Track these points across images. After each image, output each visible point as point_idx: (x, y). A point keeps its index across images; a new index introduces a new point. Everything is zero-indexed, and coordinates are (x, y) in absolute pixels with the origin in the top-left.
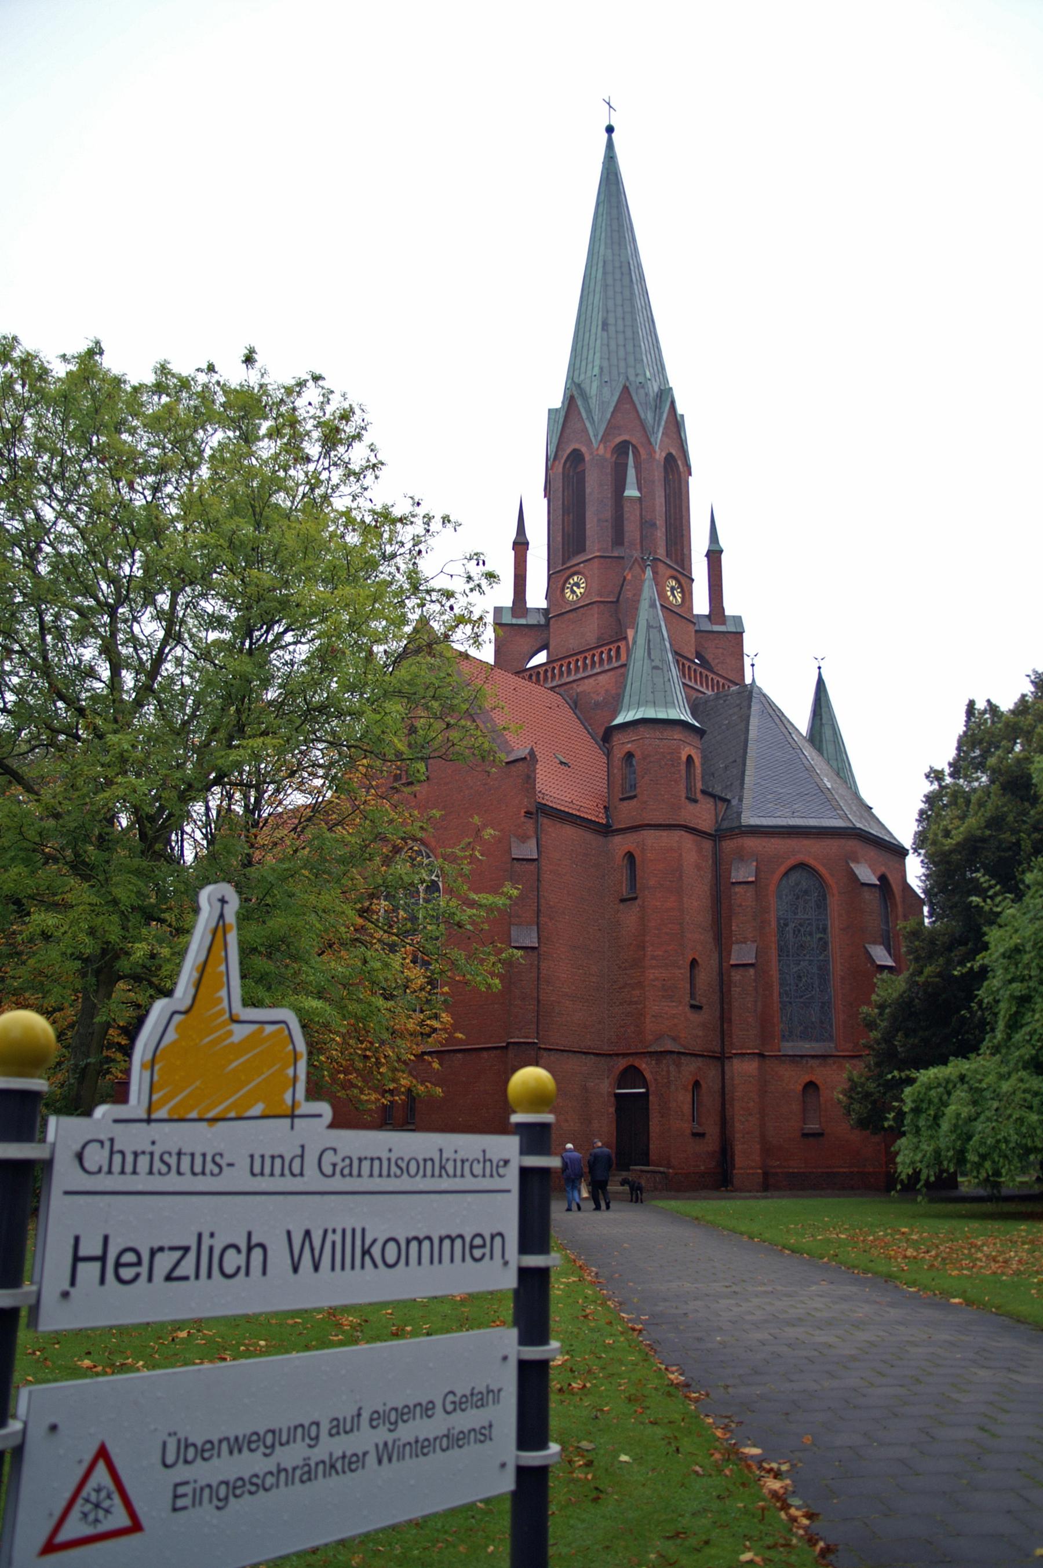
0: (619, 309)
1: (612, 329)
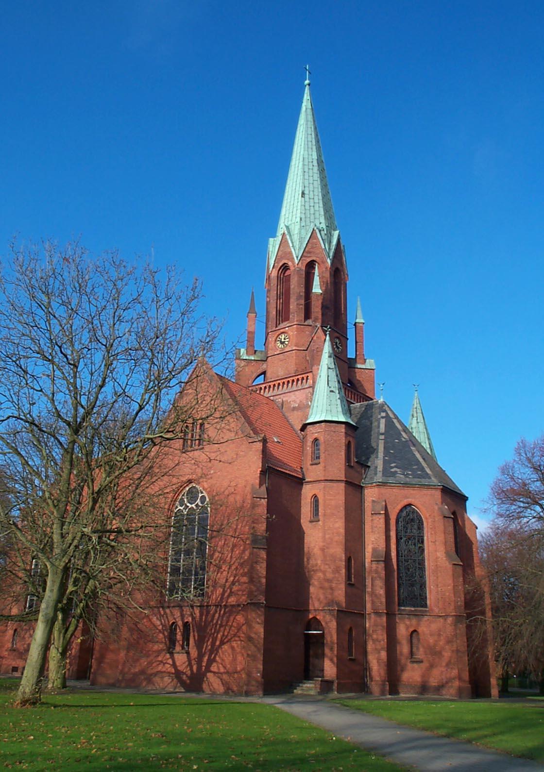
0: (311, 186)
1: (307, 196)
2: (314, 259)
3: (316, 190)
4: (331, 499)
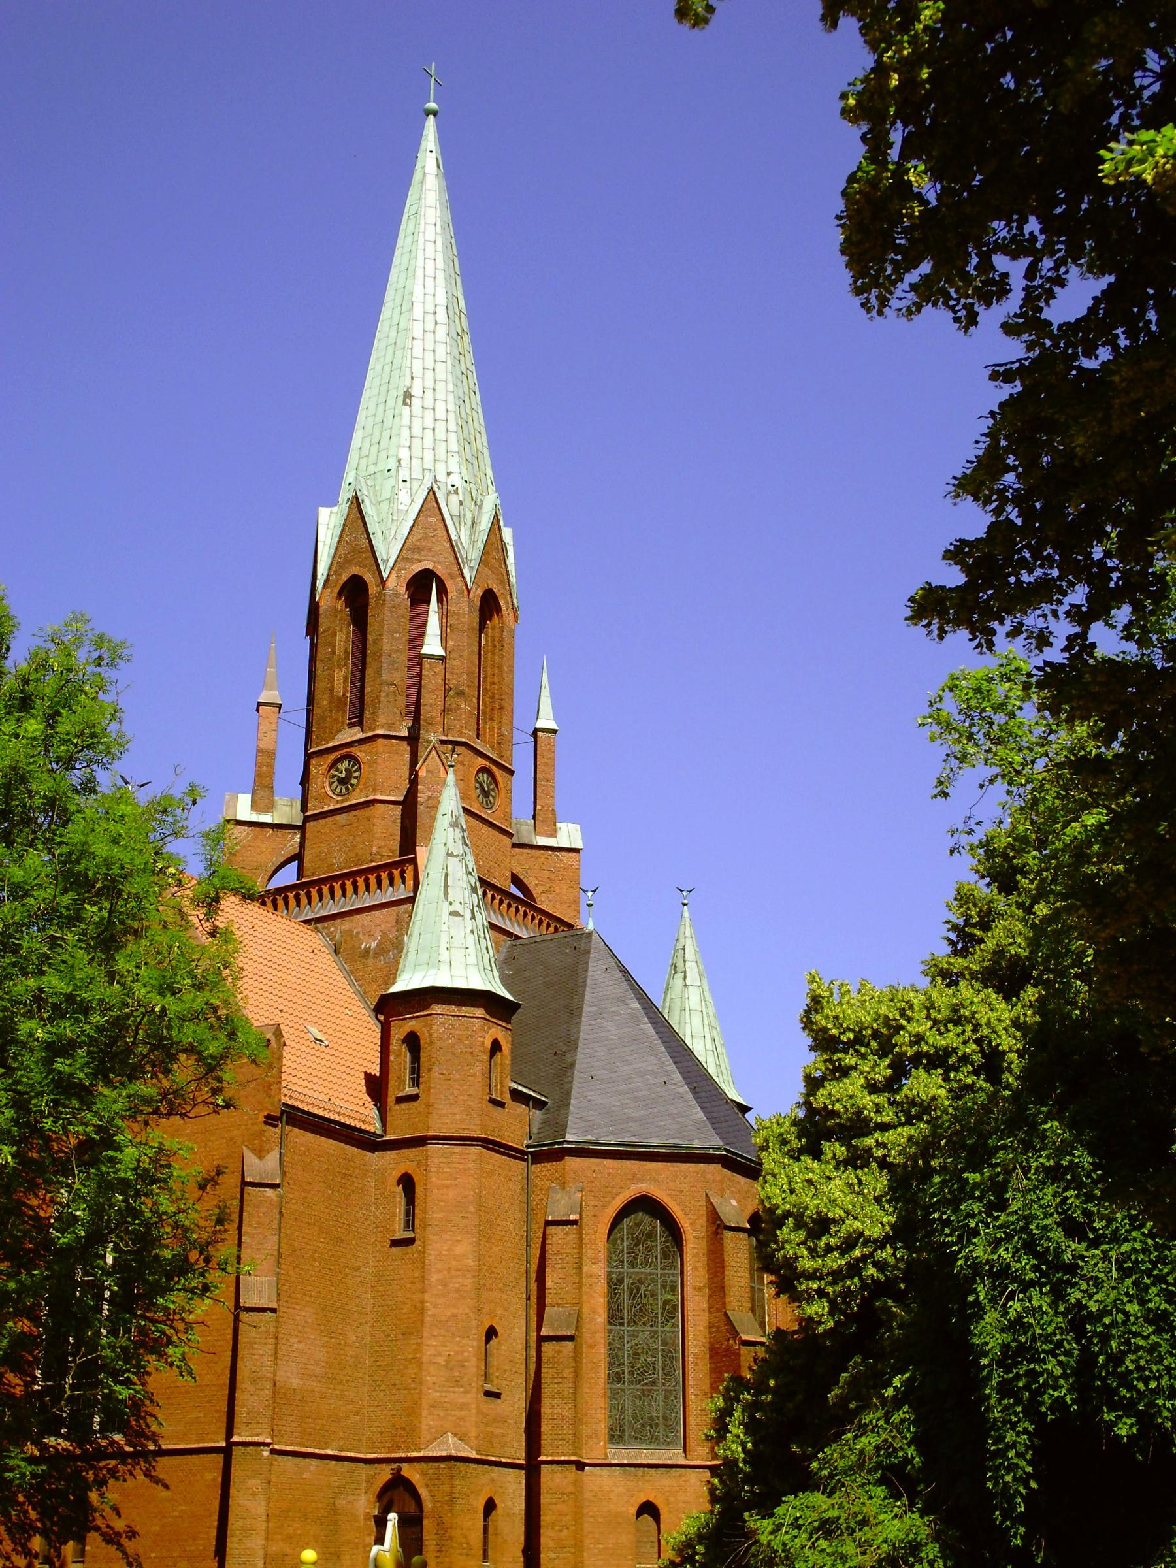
0: (429, 375)
1: (416, 402)
2: (430, 566)
3: (440, 386)
4: (447, 1187)
